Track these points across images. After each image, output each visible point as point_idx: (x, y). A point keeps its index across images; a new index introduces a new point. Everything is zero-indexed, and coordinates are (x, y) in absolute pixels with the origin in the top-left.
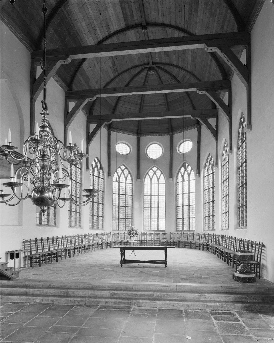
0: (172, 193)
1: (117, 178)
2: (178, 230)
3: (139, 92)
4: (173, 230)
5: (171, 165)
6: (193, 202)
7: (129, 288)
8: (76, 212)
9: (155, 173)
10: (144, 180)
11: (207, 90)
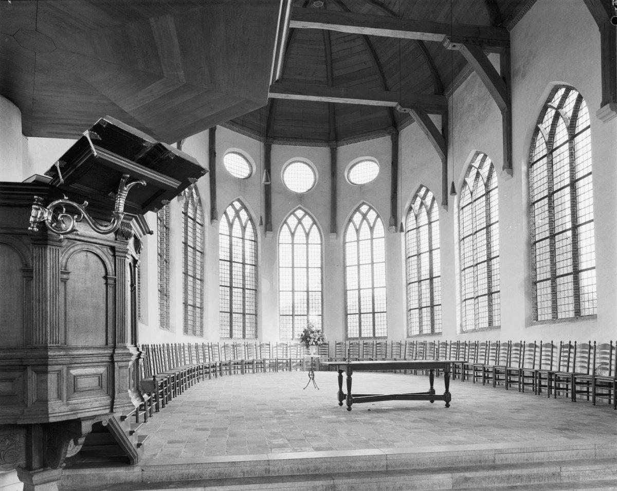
0: (333, 264)
2: (349, 336)
3: (328, 23)
5: (332, 207)
7: (486, 461)
9: (300, 221)
11: (465, 42)
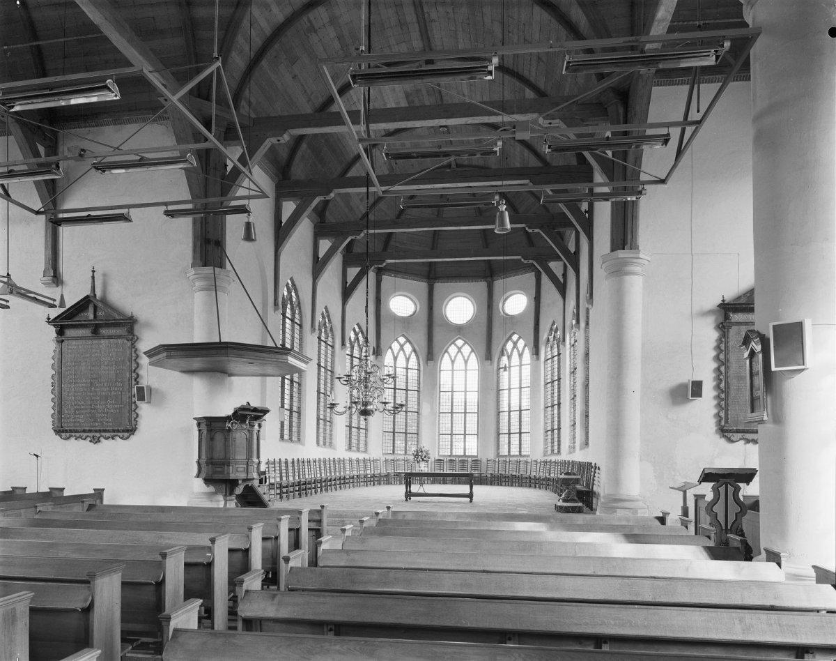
0: (491, 389)
1: (132, 65)
4: (491, 455)
5: (488, 336)
6: (525, 405)
8: (325, 420)
9: (460, 349)
10: (441, 364)
